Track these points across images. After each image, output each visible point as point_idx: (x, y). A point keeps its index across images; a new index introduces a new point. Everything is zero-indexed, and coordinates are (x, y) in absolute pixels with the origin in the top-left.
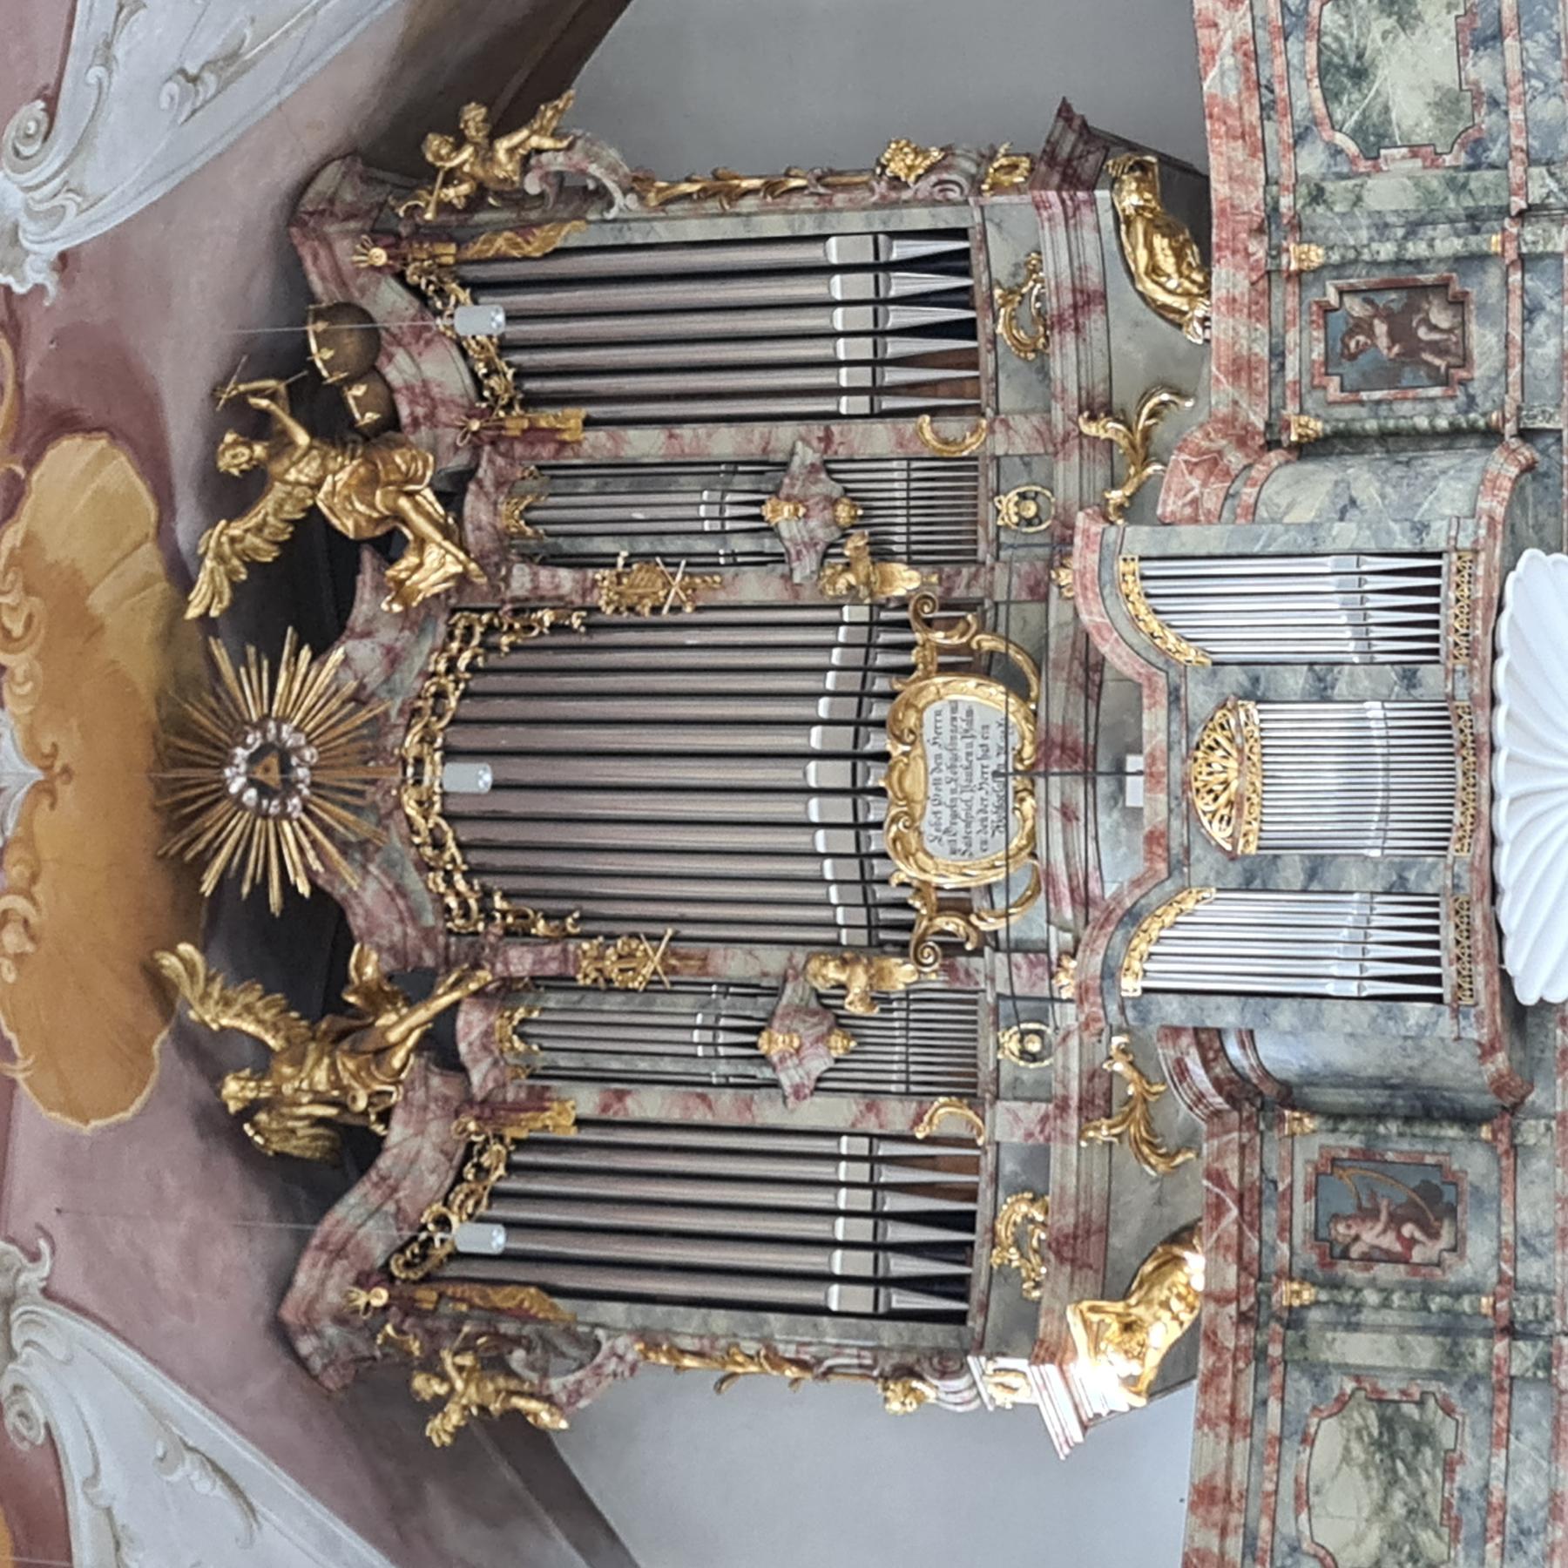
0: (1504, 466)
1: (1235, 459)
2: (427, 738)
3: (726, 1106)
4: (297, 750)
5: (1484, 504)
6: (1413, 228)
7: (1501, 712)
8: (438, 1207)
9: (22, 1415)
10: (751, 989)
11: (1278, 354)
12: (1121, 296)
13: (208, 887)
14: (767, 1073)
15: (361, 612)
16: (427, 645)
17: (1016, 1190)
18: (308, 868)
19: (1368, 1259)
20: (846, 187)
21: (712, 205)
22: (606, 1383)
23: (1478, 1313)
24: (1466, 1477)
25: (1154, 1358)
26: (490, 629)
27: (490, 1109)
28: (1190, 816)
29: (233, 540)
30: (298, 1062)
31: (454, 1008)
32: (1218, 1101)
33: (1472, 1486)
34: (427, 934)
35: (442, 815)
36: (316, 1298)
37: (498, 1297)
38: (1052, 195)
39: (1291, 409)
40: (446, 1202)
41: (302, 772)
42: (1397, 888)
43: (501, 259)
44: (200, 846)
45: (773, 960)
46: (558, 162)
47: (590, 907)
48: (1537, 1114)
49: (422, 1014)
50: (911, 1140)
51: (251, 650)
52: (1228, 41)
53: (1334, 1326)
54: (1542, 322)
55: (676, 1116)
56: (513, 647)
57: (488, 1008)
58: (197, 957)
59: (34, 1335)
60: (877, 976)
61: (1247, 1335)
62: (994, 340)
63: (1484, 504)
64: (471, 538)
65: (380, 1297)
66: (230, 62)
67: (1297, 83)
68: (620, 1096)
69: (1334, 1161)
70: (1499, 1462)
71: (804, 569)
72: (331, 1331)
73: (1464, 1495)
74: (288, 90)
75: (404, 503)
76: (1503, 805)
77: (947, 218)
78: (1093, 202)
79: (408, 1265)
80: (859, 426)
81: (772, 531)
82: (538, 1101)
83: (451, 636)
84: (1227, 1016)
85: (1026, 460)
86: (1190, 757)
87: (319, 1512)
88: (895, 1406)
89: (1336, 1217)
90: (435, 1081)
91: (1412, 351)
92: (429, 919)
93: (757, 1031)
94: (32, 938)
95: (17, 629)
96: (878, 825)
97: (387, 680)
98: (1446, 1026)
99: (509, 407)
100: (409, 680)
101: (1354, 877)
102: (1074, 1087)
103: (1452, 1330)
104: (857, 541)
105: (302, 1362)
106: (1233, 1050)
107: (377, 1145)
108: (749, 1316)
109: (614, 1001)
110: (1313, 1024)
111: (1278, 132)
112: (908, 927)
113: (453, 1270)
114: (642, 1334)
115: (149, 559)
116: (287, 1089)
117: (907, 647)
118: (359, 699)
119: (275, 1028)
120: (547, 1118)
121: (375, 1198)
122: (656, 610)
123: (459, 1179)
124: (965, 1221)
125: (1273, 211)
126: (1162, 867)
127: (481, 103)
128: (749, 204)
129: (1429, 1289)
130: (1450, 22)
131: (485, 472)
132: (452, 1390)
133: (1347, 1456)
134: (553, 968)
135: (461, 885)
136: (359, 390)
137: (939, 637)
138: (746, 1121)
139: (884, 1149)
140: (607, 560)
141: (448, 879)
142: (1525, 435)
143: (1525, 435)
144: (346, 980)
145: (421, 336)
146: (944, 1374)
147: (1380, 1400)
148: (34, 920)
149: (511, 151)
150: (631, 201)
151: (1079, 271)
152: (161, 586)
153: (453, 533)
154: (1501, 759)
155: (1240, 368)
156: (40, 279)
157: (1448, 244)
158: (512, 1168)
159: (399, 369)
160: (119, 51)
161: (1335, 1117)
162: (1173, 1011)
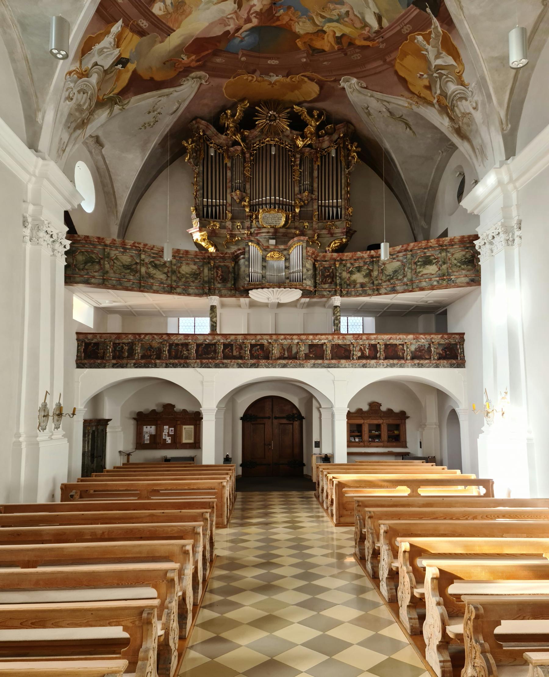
0: (312, 289)
1: (313, 256)
2: (277, 142)
3: (229, 185)
4: (275, 122)
5: (308, 287)
6: (340, 278)
7: (283, 289)
8: (214, 142)
9: (184, 81)
10: (245, 188)
11: (326, 261)
12: (332, 239)
13: (257, 108)
14: (234, 191)
15: (294, 132)
16: (289, 141)
17: (220, 224)
18: (260, 123)
19: (217, 272)
20: (347, 202)
21: (346, 183)
22: (192, 167)
23: (211, 285)
24: (192, 284)
25: (200, 243)
26: (291, 151)
27: (227, 151)
28: (271, 251)
29: (304, 112)
30: (233, 122)
31: (241, 146)
32: (236, 254)
33: (191, 284)
34: (250, 141)
35: (267, 144)
36: (200, 123)
37: (202, 151)
38: (345, 230)
39: (319, 263)
40: (214, 144)
41: (272, 123)
42: (263, 277)
43: (340, 153)
44: (262, 107)
45: (248, 192)
46: (353, 162)
47: (255, 165)
48: (235, 292)
49: (240, 141)
50: (226, 210)
51: (289, 115)
52: (364, 255)
53: (209, 268)
54: (328, 293)
55: (228, 177)
56: (289, 154)
57: (241, 150)
58: (247, 106)
59: (195, 82)
60: (247, 206)
61: (207, 257)
62: (327, 222)
63: (308, 287)
64: (304, 149)
65: (201, 134)
66: (369, 114)
67: (358, 263)
68: (230, 169)
69: (228, 268)
70: (194, 288)
71: (299, 196)
72: (196, 126)
73: (189, 284)
74: (364, 122)
75: (309, 139)
76: (273, 289)
77: (343, 216)
78: (344, 235)
79: (206, 138)
80: (317, 204)
81: (304, 192)
82: (229, 157)
83: (290, 145)
84: (247, 256)
85: (312, 226)
86: (278, 251)
87: (172, 124)
88: (192, 208)
89: (222, 268)
90: (231, 142)
91: (326, 277)
92: (252, 141)
93: (239, 189)
94: (250, 81)
95: (293, 80)
96: (266, 207)
97: (285, 136)
98: (246, 282)
99: (321, 154)
100: (285, 139)
101: (264, 272)
102: (234, 233)
103: (209, 282)
104: (302, 204)
105: (192, 121)
106: (242, 256)
107: (222, 134)
108: (202, 188)
109: (242, 169)
110: (246, 266)
111: (352, 261)
112: (253, 211)
113: (205, 145)
114: (199, 172)
115: (302, 99)
116: (230, 120)
117: (289, 211)
118: (282, 132)
119: (237, 118)
120: (226, 159)
121: (215, 133)
122: (294, 175)
123: (218, 146)
124: (216, 218)
125: (343, 260)
126: (265, 248)
127: (361, 150)
128: (346, 189)
129: (214, 279)
130: (364, 282)
131: (312, 150)
132: (190, 145)
133: (193, 269)
134: (247, 160)
135: (257, 146)
136: (324, 132)
137: (290, 215)
138: (227, 187)
139: (224, 207)
140: (300, 168)
141: (258, 144)
142: (315, 291)
143: (315, 291)
144: (245, 129)
145: (331, 141)
146: (196, 215)
147: (200, 273)
148: (253, 81)
149: (355, 155)
150: (347, 172)
151: (336, 233)
152: (298, 101)
153: (305, 146)
154: (278, 289)
155: (324, 256)
156: (342, 85)
157: (338, 282)
158: (219, 153)
159: (326, 138)
160: (372, 98)
161: (234, 268)
162: (247, 249)
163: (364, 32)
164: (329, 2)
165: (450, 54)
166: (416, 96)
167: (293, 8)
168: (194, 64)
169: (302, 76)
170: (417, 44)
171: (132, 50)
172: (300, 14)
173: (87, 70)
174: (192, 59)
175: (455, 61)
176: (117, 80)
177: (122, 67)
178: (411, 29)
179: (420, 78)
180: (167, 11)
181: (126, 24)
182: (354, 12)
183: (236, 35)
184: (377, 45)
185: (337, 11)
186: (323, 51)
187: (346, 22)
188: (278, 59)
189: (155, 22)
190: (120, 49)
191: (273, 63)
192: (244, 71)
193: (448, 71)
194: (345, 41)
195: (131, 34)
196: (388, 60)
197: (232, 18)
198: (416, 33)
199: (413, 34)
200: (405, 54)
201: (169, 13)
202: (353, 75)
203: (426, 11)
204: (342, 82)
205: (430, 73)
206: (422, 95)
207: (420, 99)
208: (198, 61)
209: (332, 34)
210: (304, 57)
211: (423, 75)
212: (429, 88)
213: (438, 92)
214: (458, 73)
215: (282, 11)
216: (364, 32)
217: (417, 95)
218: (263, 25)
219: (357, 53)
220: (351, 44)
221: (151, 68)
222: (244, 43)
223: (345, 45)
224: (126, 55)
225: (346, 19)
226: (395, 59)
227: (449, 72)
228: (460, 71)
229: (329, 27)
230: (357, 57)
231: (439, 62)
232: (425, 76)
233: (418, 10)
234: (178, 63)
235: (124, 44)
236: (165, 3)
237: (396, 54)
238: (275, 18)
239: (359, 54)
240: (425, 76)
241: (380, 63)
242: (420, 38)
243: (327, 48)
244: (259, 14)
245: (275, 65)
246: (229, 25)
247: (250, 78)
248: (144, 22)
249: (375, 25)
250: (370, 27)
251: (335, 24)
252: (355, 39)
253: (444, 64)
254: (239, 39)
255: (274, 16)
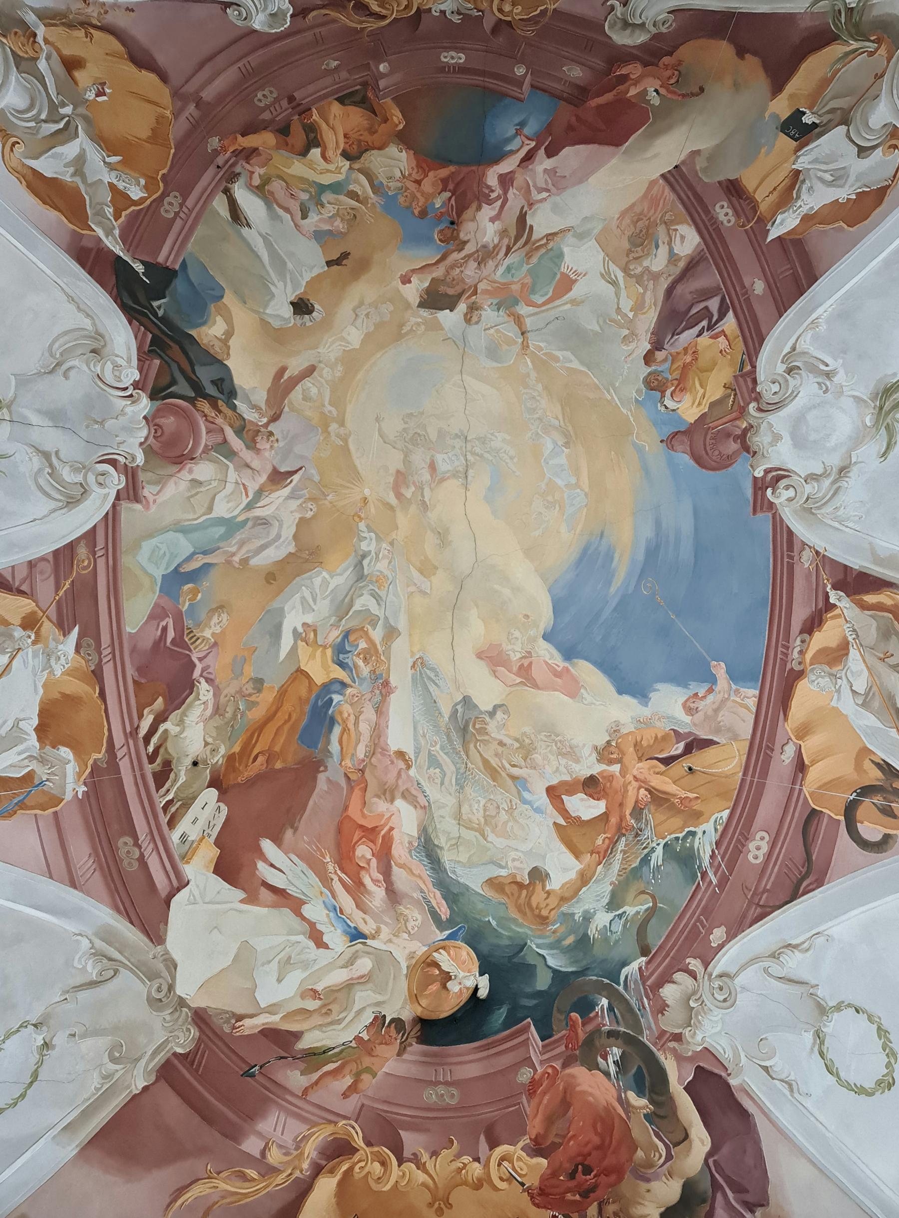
163: (262, 171)
164: (346, 233)
165: (54, 183)
166: (95, 22)
167: (416, 212)
168: (634, 70)
169: (384, 17)
170: (137, 175)
171: (767, 154)
172: (401, 199)
173: (890, 147)
174: (635, 85)
175: (34, 171)
176: (825, 82)
177: (804, 113)
178: (162, 210)
179: (103, 84)
180: (668, 230)
181: (763, 223)
182: (293, 220)
183: (533, 144)
184: (226, 142)
185: (326, 216)
186: (341, 100)
187: (303, 191)
188: (444, 69)
189: (699, 209)
190: (794, 167)
191: (453, 53)
192: (519, 32)
193: (40, 136)
194: (298, 136)
195: (758, 197)
196: (192, 108)
197: (540, 190)
198: (148, 202)
199: (154, 197)
200: (157, 136)
201: (665, 223)
202: (266, 40)
203: (143, 262)
204: (288, 9)
205: (81, 110)
206: (81, 33)
207: (82, 18)
208: (624, 79)
209: (330, 153)
210: (383, 76)
211: (97, 95)
212: (71, 65)
213: (42, 65)
214: (13, 145)
215: (437, 206)
216: (262, 171)
217: (95, 27)
218: (474, 168)
219: (267, 107)
220: (284, 131)
221: (736, 86)
222: (517, 120)
223: (296, 128)
224: (785, 142)
225: (304, 196)
226: (176, 115)
227: (38, 131)
228: (12, 150)
229: (338, 170)
230: (264, 97)
231: (70, 150)
232: (90, 95)
233: (161, 259)
234: (672, 81)
235: (781, 176)
236: (671, 250)
237: (176, 130)
238: (451, 186)
239: (262, 105)
240: (90, 95)
241: (208, 94)
242: (136, 193)
243: (336, 109)
244: (483, 198)
245: (447, 49)
246: (545, 170)
247: (507, 8)
248: (722, 217)
249: (241, 193)
250: (250, 187)
251: (326, 180)
252: (278, 147)
253: (58, 149)
254: (527, 131)
255: (453, 193)
